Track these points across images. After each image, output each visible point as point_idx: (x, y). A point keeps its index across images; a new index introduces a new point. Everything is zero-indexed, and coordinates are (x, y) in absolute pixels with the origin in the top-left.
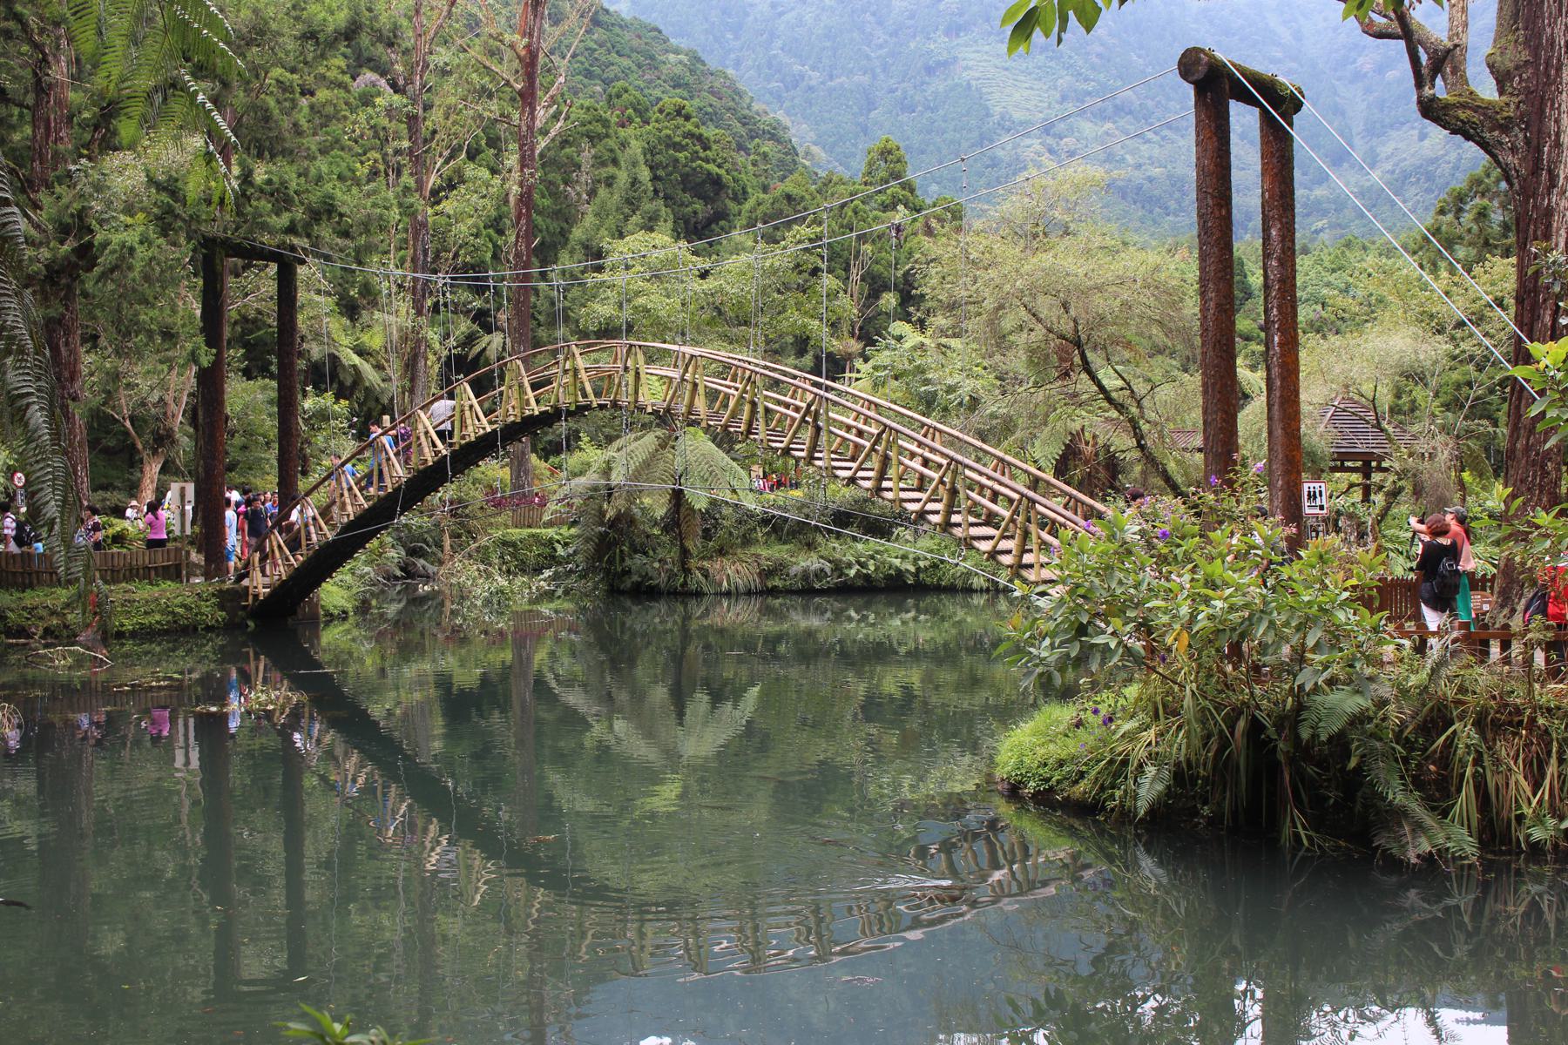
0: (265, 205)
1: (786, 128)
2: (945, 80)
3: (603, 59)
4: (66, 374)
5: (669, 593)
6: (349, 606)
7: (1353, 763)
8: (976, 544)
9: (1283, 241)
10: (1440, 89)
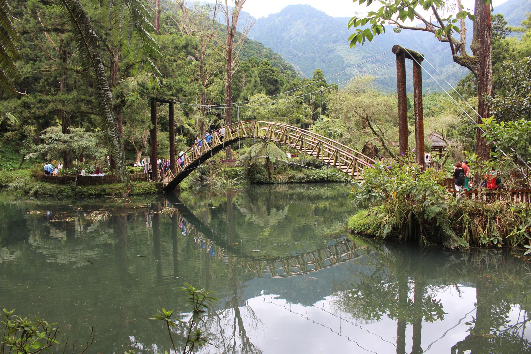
1: (293, 67)
6: (187, 187)
7: (438, 224)
8: (342, 170)
9: (419, 93)
10: (459, 54)
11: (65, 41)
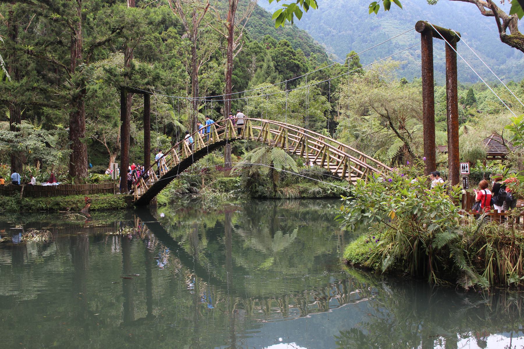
0: (138, 76)
1: (324, 48)
2: (377, 32)
3: (265, 27)
4: (81, 129)
5: (270, 198)
6: (167, 202)
7: (451, 256)
8: (353, 183)
9: (453, 84)
10: (508, 32)
11: (15, 13)
